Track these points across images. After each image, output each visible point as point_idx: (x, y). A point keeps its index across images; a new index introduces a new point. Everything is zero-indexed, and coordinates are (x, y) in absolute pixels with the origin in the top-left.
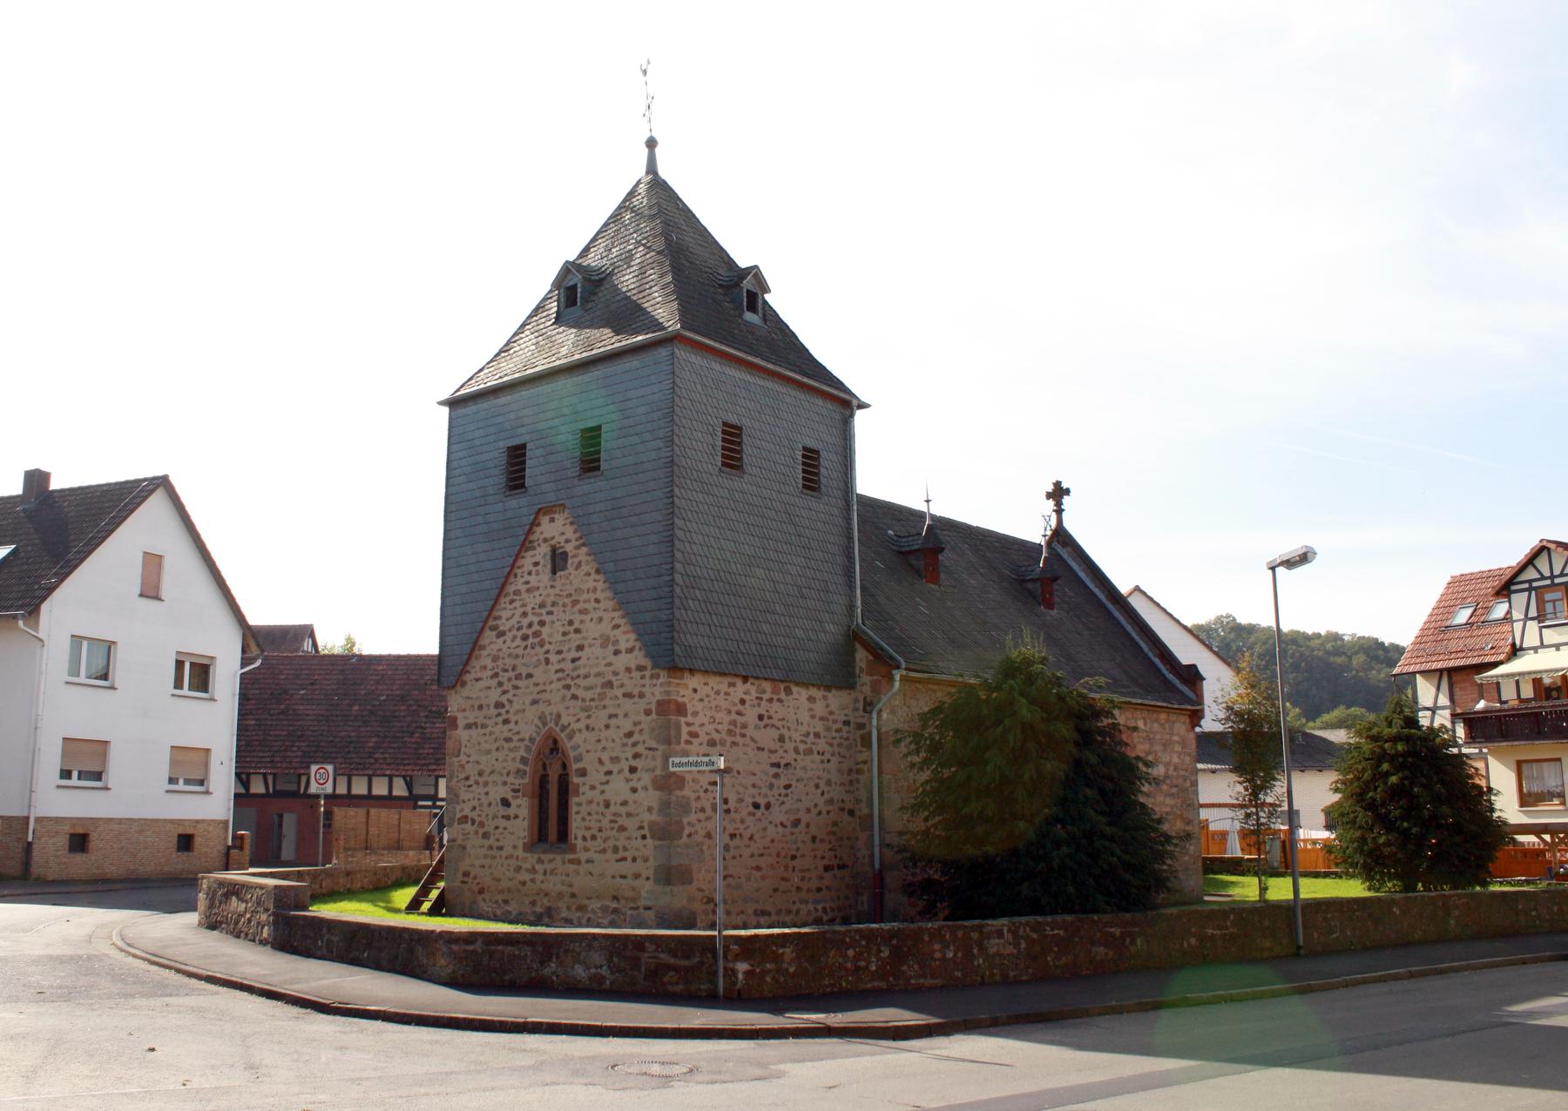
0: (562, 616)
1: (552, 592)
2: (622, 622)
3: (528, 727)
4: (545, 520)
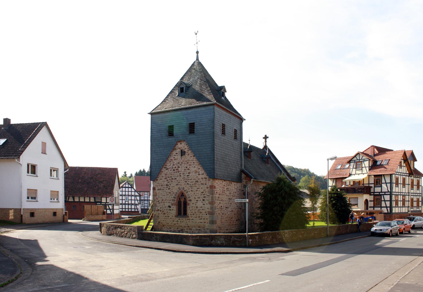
0: (184, 166)
1: (181, 160)
2: (200, 168)
3: (175, 190)
4: (179, 144)
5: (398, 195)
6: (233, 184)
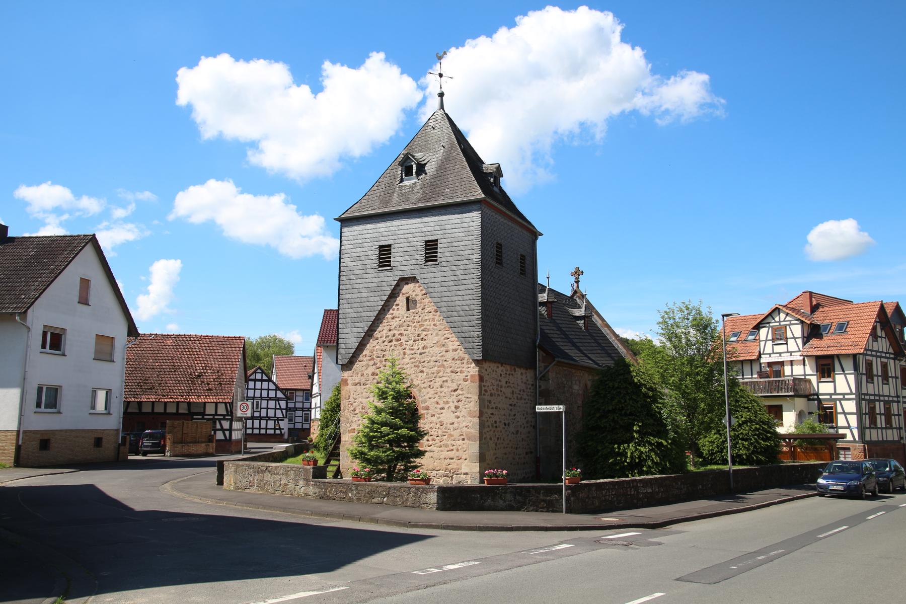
5: (875, 401)
6: (519, 371)
